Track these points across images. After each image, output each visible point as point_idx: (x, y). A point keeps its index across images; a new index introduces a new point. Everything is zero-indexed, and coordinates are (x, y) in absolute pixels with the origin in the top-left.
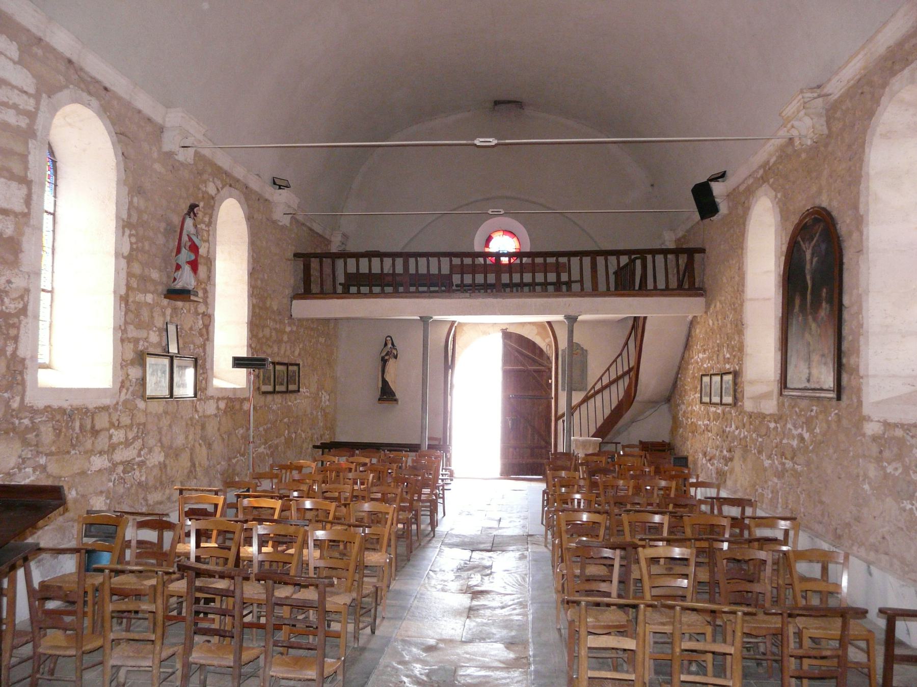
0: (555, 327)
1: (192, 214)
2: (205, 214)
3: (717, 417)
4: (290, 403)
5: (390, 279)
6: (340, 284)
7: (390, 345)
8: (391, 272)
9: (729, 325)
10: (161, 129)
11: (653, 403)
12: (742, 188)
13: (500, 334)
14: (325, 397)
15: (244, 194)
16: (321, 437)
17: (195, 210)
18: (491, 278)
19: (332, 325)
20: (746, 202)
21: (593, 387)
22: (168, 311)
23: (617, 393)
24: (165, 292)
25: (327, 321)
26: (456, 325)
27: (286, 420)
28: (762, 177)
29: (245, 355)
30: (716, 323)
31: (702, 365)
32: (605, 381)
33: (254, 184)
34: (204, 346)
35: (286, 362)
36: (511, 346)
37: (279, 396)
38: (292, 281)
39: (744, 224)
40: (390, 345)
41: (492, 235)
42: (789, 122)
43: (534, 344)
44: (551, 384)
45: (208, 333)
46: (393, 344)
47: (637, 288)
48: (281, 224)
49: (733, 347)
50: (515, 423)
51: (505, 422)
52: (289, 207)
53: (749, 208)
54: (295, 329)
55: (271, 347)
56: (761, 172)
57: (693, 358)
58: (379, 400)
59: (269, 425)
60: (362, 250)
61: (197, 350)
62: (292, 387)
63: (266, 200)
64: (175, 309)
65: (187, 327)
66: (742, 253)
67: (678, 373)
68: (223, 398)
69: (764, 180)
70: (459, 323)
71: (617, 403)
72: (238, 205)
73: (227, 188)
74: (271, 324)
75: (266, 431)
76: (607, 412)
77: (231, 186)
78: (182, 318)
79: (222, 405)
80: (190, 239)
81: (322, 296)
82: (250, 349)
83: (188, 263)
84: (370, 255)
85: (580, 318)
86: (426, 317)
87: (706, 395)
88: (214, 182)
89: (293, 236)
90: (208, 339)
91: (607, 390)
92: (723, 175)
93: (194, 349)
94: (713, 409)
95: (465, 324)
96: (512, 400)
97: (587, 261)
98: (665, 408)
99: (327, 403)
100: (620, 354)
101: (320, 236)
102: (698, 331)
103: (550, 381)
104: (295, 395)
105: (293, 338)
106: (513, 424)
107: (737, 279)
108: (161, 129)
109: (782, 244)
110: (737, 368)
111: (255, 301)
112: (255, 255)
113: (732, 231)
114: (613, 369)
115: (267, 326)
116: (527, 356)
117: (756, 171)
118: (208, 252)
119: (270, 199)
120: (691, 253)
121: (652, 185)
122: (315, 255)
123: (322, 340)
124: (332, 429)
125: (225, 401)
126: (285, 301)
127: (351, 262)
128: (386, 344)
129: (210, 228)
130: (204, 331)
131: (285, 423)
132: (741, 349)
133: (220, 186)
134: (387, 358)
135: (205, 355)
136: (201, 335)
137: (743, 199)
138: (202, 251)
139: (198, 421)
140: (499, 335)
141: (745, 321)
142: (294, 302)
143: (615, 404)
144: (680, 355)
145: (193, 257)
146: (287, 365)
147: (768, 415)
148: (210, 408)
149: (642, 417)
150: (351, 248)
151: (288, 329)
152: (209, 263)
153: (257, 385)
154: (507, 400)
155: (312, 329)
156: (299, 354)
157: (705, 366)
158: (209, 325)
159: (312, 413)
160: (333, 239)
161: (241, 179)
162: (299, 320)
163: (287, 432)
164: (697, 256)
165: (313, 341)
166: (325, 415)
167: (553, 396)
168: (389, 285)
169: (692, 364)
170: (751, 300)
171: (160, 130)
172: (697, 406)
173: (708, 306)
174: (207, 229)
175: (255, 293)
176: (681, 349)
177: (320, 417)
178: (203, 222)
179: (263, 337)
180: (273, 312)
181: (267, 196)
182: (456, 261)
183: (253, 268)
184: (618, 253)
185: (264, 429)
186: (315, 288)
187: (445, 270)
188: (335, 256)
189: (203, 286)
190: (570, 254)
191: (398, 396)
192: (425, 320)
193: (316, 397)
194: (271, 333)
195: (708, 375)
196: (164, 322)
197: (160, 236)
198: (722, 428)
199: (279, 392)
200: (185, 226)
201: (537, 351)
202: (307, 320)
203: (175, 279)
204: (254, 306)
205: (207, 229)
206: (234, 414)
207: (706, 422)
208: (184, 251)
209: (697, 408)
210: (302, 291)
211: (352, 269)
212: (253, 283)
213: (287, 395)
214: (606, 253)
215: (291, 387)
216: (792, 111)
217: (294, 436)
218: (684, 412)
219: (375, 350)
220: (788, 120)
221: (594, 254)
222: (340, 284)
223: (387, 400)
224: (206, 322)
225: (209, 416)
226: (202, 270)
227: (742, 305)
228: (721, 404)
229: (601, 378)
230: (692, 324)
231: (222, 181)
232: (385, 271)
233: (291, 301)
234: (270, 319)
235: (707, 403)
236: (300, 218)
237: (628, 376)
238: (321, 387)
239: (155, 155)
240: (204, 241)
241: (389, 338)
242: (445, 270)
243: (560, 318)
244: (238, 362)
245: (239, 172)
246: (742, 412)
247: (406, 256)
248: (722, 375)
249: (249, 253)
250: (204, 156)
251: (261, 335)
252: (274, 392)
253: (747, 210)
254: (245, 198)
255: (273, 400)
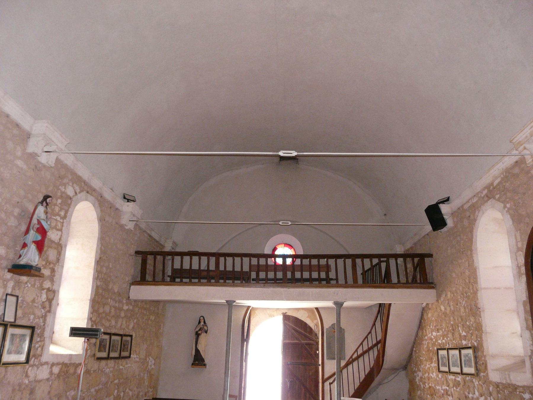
0: (320, 310)
1: (44, 203)
2: (61, 209)
3: (457, 384)
4: (121, 367)
5: (205, 274)
6: (169, 276)
7: (202, 323)
8: (206, 269)
9: (462, 310)
10: (28, 136)
11: (394, 370)
12: (466, 207)
13: (281, 317)
14: (151, 361)
15: (99, 201)
16: (146, 394)
17: (48, 200)
18: (280, 275)
19: (161, 307)
20: (472, 216)
21: (351, 357)
22: (11, 284)
23: (368, 361)
24: (10, 267)
25: (158, 302)
26: (250, 308)
27: (116, 381)
28: (487, 196)
29: (85, 327)
30: (448, 308)
31: (436, 341)
32: (360, 351)
33: (108, 195)
34: (44, 317)
35: (122, 333)
36: (289, 325)
37: (112, 361)
38: (132, 271)
39: (471, 232)
40: (202, 323)
41: (277, 247)
42: (522, 145)
43: (306, 324)
44: (318, 354)
45: (50, 306)
46: (205, 322)
47: (386, 283)
48: (127, 228)
49: (469, 327)
50: (292, 383)
51: (284, 383)
52: (134, 215)
53: (475, 220)
54: (131, 307)
55: (110, 321)
56: (486, 192)
57: (426, 335)
58: (192, 364)
59: (100, 386)
60: (186, 250)
61: (37, 320)
62: (124, 354)
63: (117, 209)
64: (18, 283)
65: (29, 299)
66: (471, 254)
67: (413, 347)
68: (58, 364)
69: (489, 197)
70: (253, 308)
71: (369, 369)
72: (93, 208)
73: (84, 194)
74: (111, 302)
75: (97, 391)
76: (363, 377)
77: (88, 192)
78: (25, 292)
79: (56, 370)
80: (39, 222)
81: (154, 283)
82: (90, 322)
83: (35, 242)
84: (191, 254)
85: (346, 304)
86: (230, 301)
87: (444, 365)
88: (73, 186)
89: (136, 238)
90: (49, 311)
91: (362, 358)
92: (447, 200)
93: (34, 319)
94: (451, 377)
95: (256, 309)
96: (290, 366)
97: (349, 262)
98: (403, 373)
99: (153, 366)
100: (370, 332)
101: (157, 242)
102: (430, 315)
103: (317, 352)
104: (127, 360)
105: (129, 315)
106: (290, 385)
107: (467, 273)
108: (28, 136)
109: (517, 242)
110: (476, 344)
111: (99, 283)
112: (103, 248)
113: (459, 238)
114: (365, 343)
115: (108, 304)
116: (300, 333)
117: (481, 192)
118: (60, 239)
119: (120, 208)
120: (422, 257)
121: (385, 215)
122: (151, 253)
123: (152, 318)
124: (155, 388)
125: (60, 366)
126: (125, 286)
127: (177, 259)
128: (200, 322)
129: (65, 220)
130: (47, 304)
131: (115, 384)
132: (479, 328)
133: (78, 191)
134: (200, 332)
135: (44, 325)
136: (44, 308)
137: (468, 214)
138: (52, 235)
139: (27, 386)
140: (281, 317)
141: (480, 305)
142: (132, 287)
143: (368, 370)
144: (414, 334)
145: (39, 238)
146: (121, 336)
147: (521, 387)
148: (43, 373)
149: (386, 381)
150: (178, 250)
151: (125, 307)
152: (60, 248)
153: (93, 353)
154: (286, 366)
155: (145, 309)
156: (133, 327)
157: (440, 341)
158: (53, 299)
159: (139, 375)
160: (166, 245)
161: (98, 189)
162: (135, 301)
163: (116, 391)
164: (427, 260)
165: (146, 317)
166: (151, 376)
167: (320, 363)
168: (204, 278)
169: (426, 340)
170: (485, 288)
171: (26, 136)
172: (434, 374)
173: (439, 296)
174: (62, 221)
175: (100, 277)
176: (416, 329)
177: (146, 378)
178: (59, 215)
179: (104, 312)
180: (115, 293)
181: (118, 206)
182: (254, 261)
183: (100, 258)
184: (371, 257)
185: (96, 391)
186: (149, 278)
187: (246, 268)
188: (165, 254)
189: (51, 266)
190: (337, 257)
191: (206, 361)
192: (230, 304)
193: (144, 362)
194: (110, 309)
195: (445, 349)
196: (4, 293)
197: (12, 219)
198: (464, 394)
199: (112, 358)
200: (36, 212)
201: (308, 329)
202: (142, 301)
203: (20, 256)
204: (97, 287)
205: (62, 221)
206: (68, 377)
207: (445, 387)
208: (32, 233)
209: (434, 375)
210: (139, 279)
211: (177, 266)
212: (99, 269)
213: (120, 361)
214: (363, 257)
215: (124, 354)
216: (524, 136)
217: (122, 394)
218: (421, 378)
219: (191, 327)
220: (520, 144)
221: (354, 257)
222: (169, 276)
223: (198, 365)
224: (51, 297)
225: (40, 381)
226: (52, 254)
227: (475, 293)
228: (462, 373)
229: (356, 350)
230: (424, 311)
231: (80, 187)
232: (202, 268)
233: (130, 287)
234: (111, 299)
235: (446, 372)
236: (143, 226)
237: (376, 347)
238: (149, 354)
239: (19, 154)
240: (55, 228)
241: (202, 318)
242: (246, 268)
243: (329, 304)
244: (75, 332)
245: (96, 184)
246: (487, 381)
247: (218, 255)
248: (460, 349)
249: (98, 246)
250: (67, 165)
251: (101, 311)
252: (108, 358)
253: (473, 222)
254: (99, 204)
255: (107, 365)
